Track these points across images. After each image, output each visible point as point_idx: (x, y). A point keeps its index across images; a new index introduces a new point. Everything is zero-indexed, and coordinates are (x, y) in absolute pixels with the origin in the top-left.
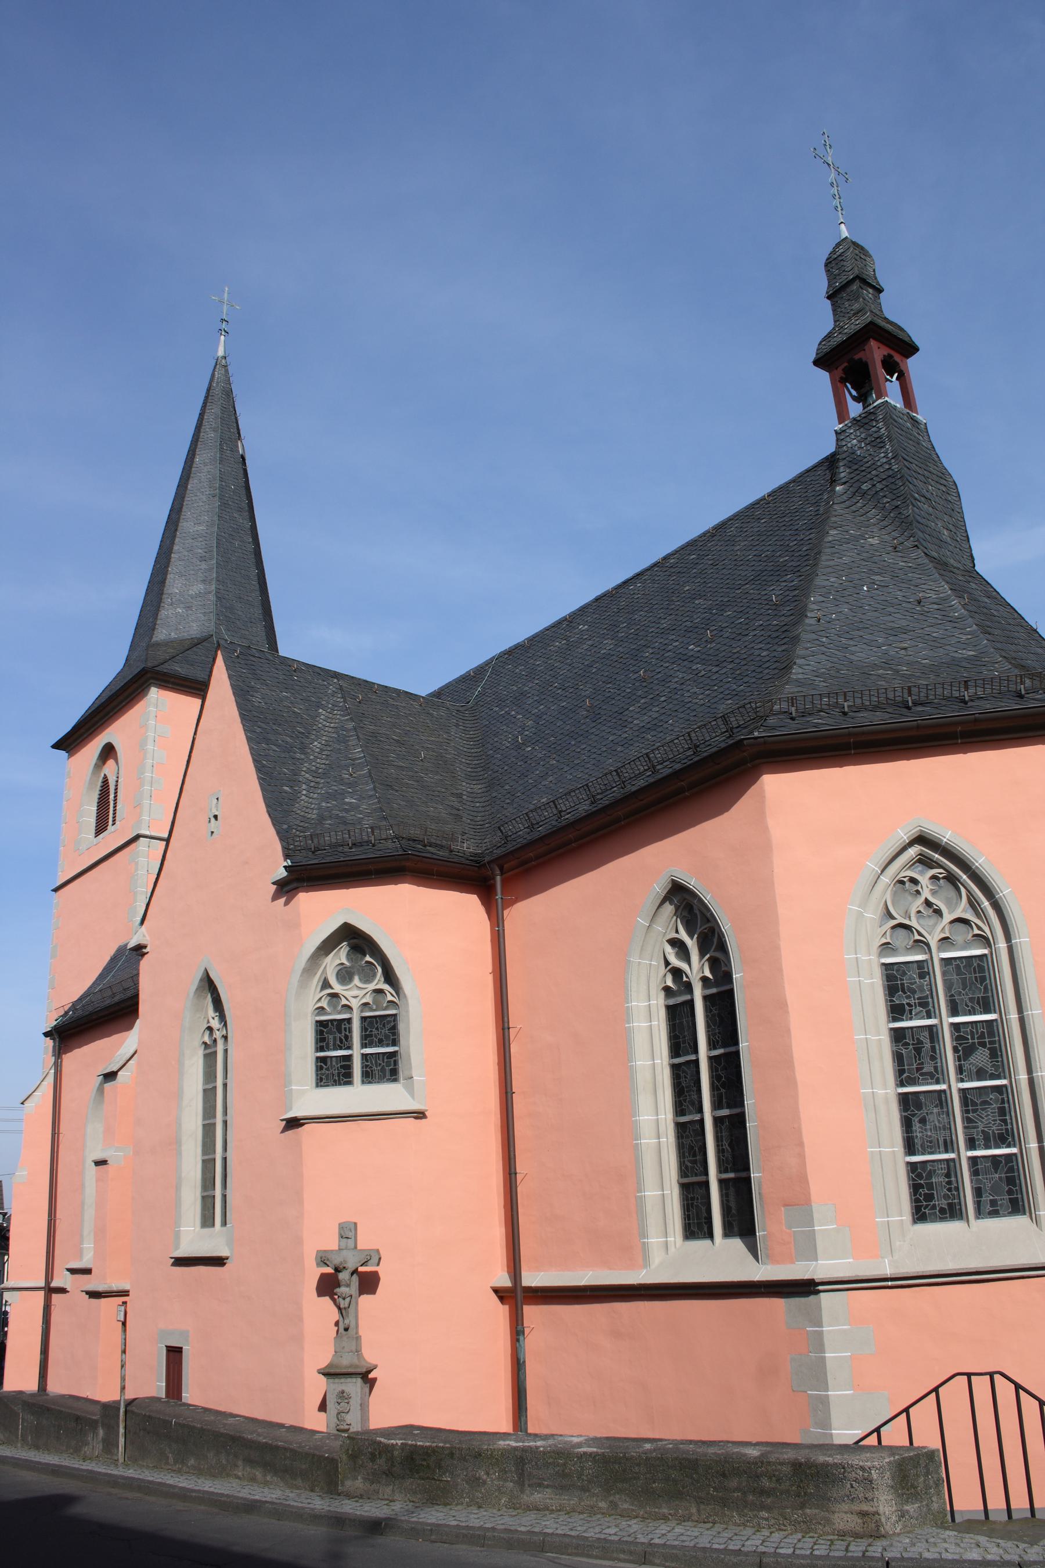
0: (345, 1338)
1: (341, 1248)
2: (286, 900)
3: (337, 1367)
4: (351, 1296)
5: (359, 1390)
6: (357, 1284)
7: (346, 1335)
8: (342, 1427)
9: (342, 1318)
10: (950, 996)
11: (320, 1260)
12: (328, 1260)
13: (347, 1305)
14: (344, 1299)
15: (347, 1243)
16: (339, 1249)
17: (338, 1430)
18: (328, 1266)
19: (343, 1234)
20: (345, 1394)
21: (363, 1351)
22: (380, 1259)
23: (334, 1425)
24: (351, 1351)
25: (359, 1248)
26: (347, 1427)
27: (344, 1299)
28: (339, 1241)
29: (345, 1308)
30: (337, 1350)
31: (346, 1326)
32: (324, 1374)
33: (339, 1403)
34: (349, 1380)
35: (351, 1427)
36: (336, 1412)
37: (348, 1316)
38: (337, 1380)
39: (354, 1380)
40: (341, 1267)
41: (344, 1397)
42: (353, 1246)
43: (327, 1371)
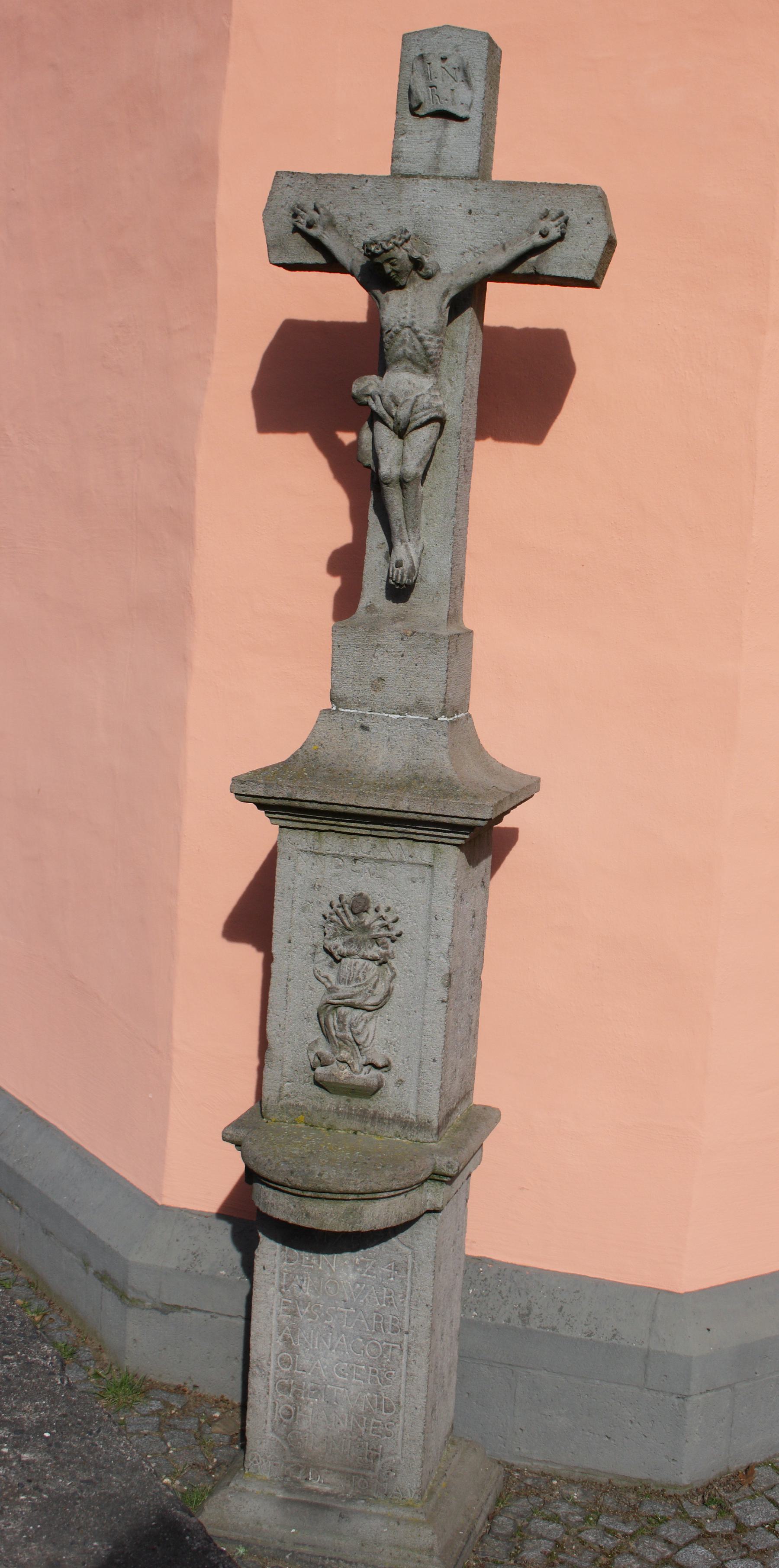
0: (390, 637)
1: (405, 167)
2: (493, 861)
3: (334, 776)
4: (441, 421)
5: (445, 905)
6: (475, 368)
7: (395, 619)
8: (343, 1074)
9: (375, 535)
10: (596, 1483)
11: (288, 221)
12: (331, 224)
13: (412, 467)
14: (402, 432)
15: (441, 143)
16: (396, 175)
17: (317, 1083)
18: (482, 1145)
19: (422, 92)
20: (369, 918)
21: (475, 708)
22: (611, 243)
23: (305, 1058)
24: (420, 707)
25: (497, 174)
26: (369, 1076)
27: (402, 432)
28: (399, 132)
29: (403, 482)
30: (345, 690)
31: (401, 575)
32: (267, 806)
33: (336, 959)
34: (396, 849)
35: (389, 1079)
36: (319, 995)
37: (412, 523)
38: (332, 843)
39: (424, 853)
40: (401, 254)
41: (366, 929)
42: (468, 163)
43: (283, 791)
